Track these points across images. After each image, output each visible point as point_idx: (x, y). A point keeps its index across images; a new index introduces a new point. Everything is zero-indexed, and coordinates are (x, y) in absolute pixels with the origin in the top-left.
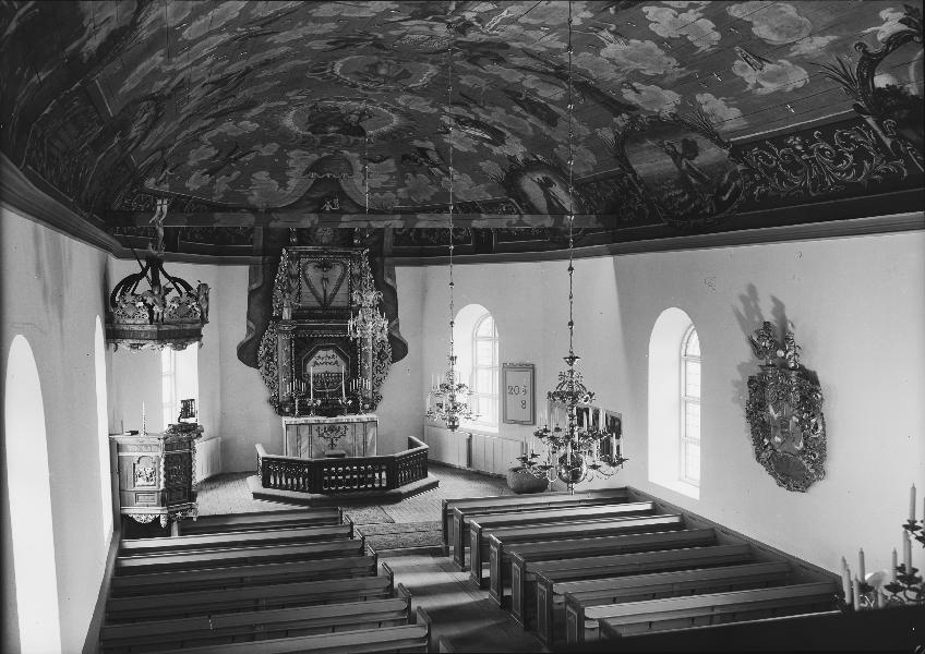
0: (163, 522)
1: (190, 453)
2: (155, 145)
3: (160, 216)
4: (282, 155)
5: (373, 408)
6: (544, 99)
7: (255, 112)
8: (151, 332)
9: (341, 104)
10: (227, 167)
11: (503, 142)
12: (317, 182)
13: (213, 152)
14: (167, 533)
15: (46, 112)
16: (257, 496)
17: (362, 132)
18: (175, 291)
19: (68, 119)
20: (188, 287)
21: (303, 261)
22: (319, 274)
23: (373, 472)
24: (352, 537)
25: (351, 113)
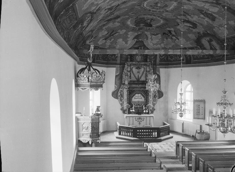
0: (90, 143)
1: (99, 122)
2: (90, 29)
3: (91, 50)
4: (126, 34)
5: (152, 112)
6: (211, 12)
7: (119, 19)
8: (88, 85)
9: (145, 16)
10: (110, 37)
11: (196, 27)
12: (137, 42)
13: (106, 33)
14: (91, 146)
15: (62, 13)
16: (117, 138)
17: (151, 26)
18: (95, 73)
19: (68, 17)
20: (99, 72)
21: (132, 67)
22: (137, 70)
23: (153, 132)
24: (147, 151)
25: (148, 20)
